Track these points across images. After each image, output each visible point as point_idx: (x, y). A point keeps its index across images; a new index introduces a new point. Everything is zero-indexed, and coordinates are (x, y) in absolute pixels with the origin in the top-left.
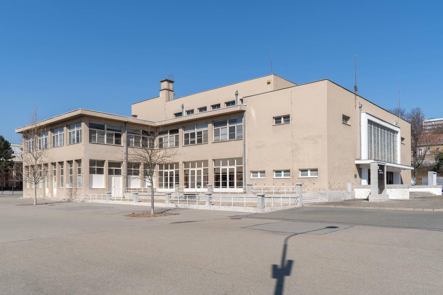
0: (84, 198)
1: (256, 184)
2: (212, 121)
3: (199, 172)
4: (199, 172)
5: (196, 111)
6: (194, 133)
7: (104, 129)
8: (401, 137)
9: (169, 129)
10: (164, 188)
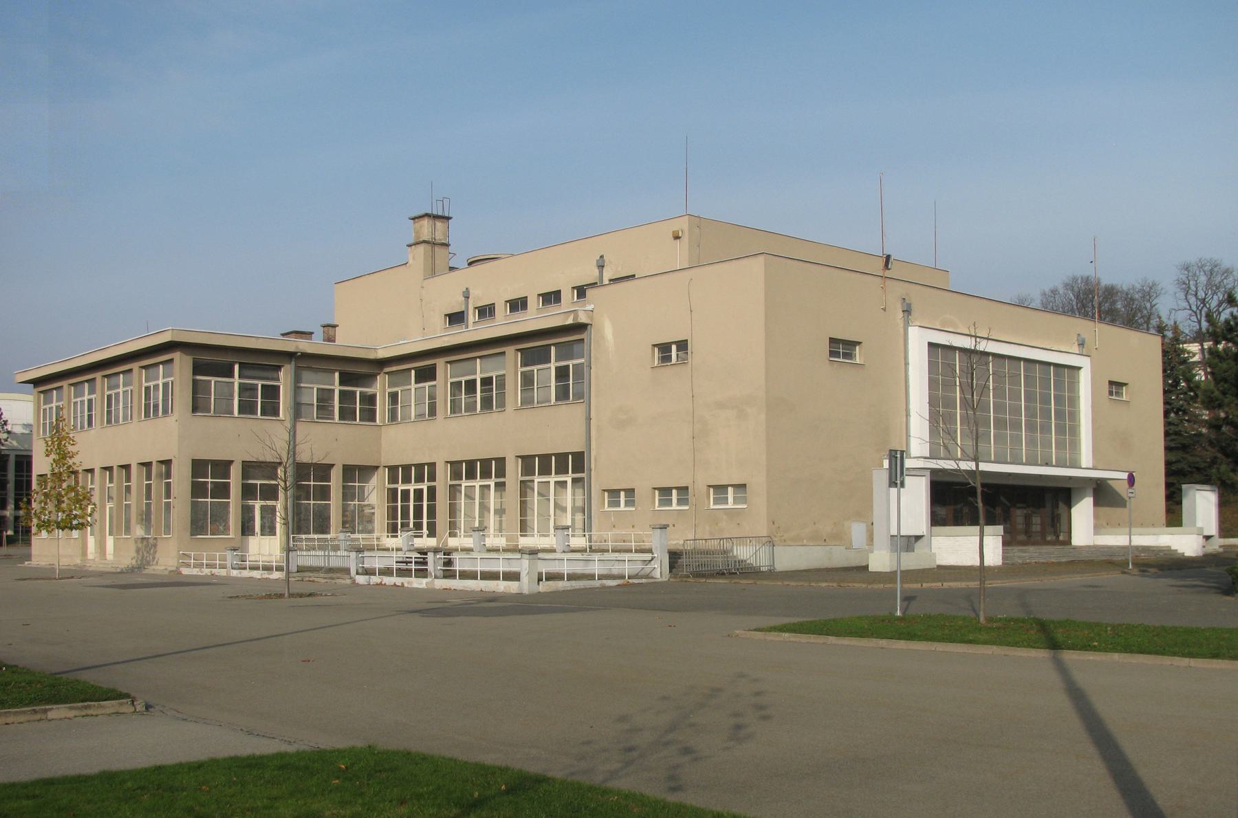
1: (614, 526)
3: (419, 493)
4: (419, 493)
5: (501, 311)
6: (475, 380)
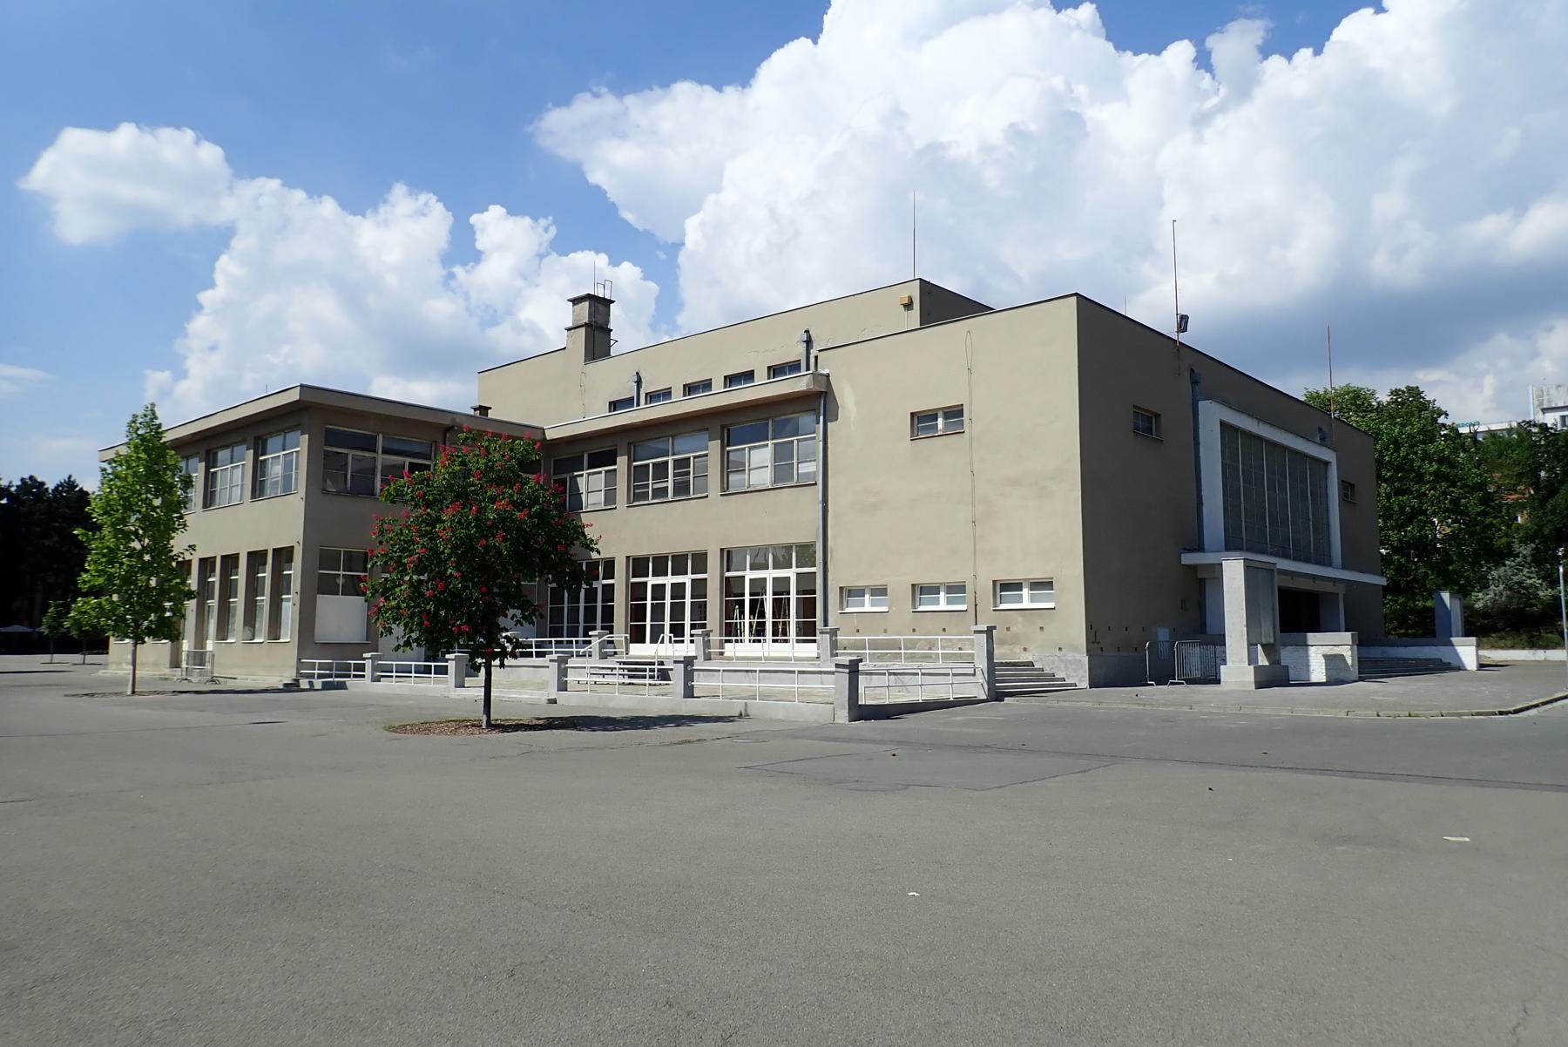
0: (295, 674)
1: (858, 631)
2: (723, 427)
4: (678, 590)
7: (374, 451)
8: (1343, 481)
9: (586, 451)
10: (747, 641)
